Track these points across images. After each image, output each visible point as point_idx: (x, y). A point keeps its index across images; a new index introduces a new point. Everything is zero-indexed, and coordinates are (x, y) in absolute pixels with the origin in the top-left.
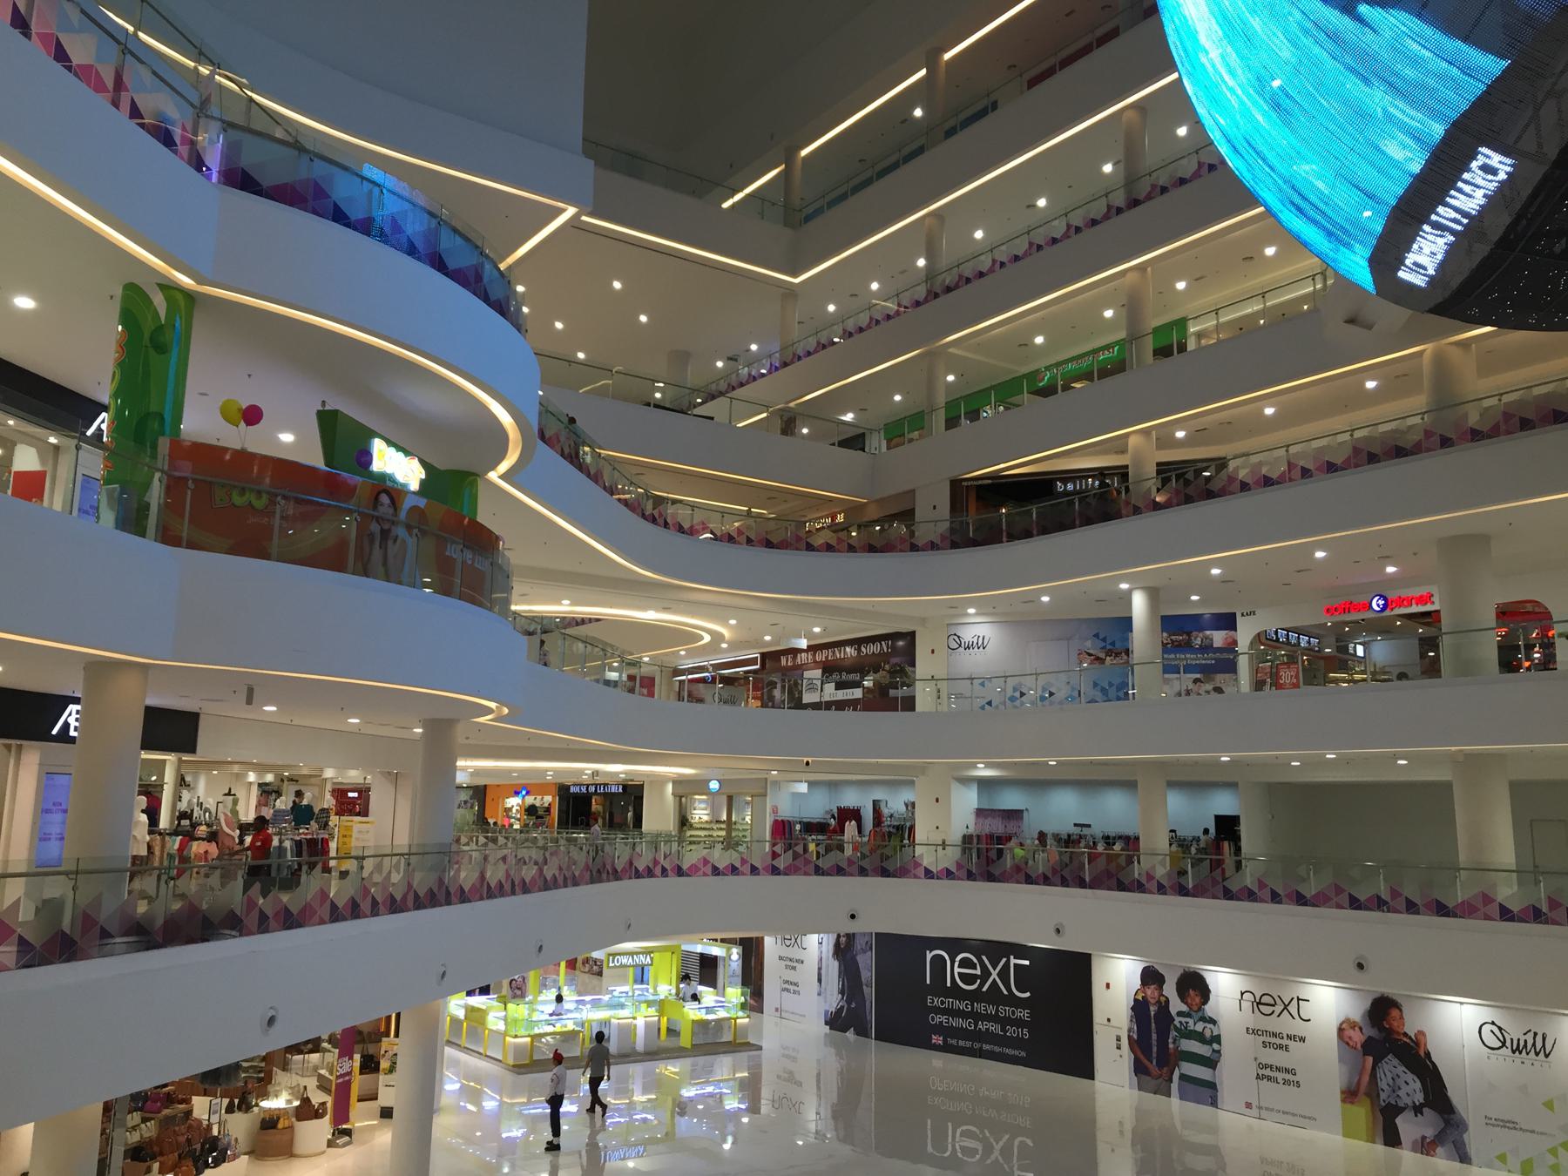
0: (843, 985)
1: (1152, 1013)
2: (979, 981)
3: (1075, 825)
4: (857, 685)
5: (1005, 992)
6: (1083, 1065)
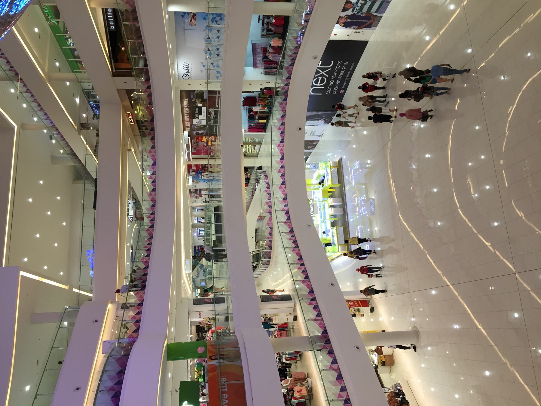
0: (316, 119)
1: (350, 21)
2: (324, 78)
3: (259, 22)
4: (200, 108)
5: (330, 69)
6: (364, 44)
